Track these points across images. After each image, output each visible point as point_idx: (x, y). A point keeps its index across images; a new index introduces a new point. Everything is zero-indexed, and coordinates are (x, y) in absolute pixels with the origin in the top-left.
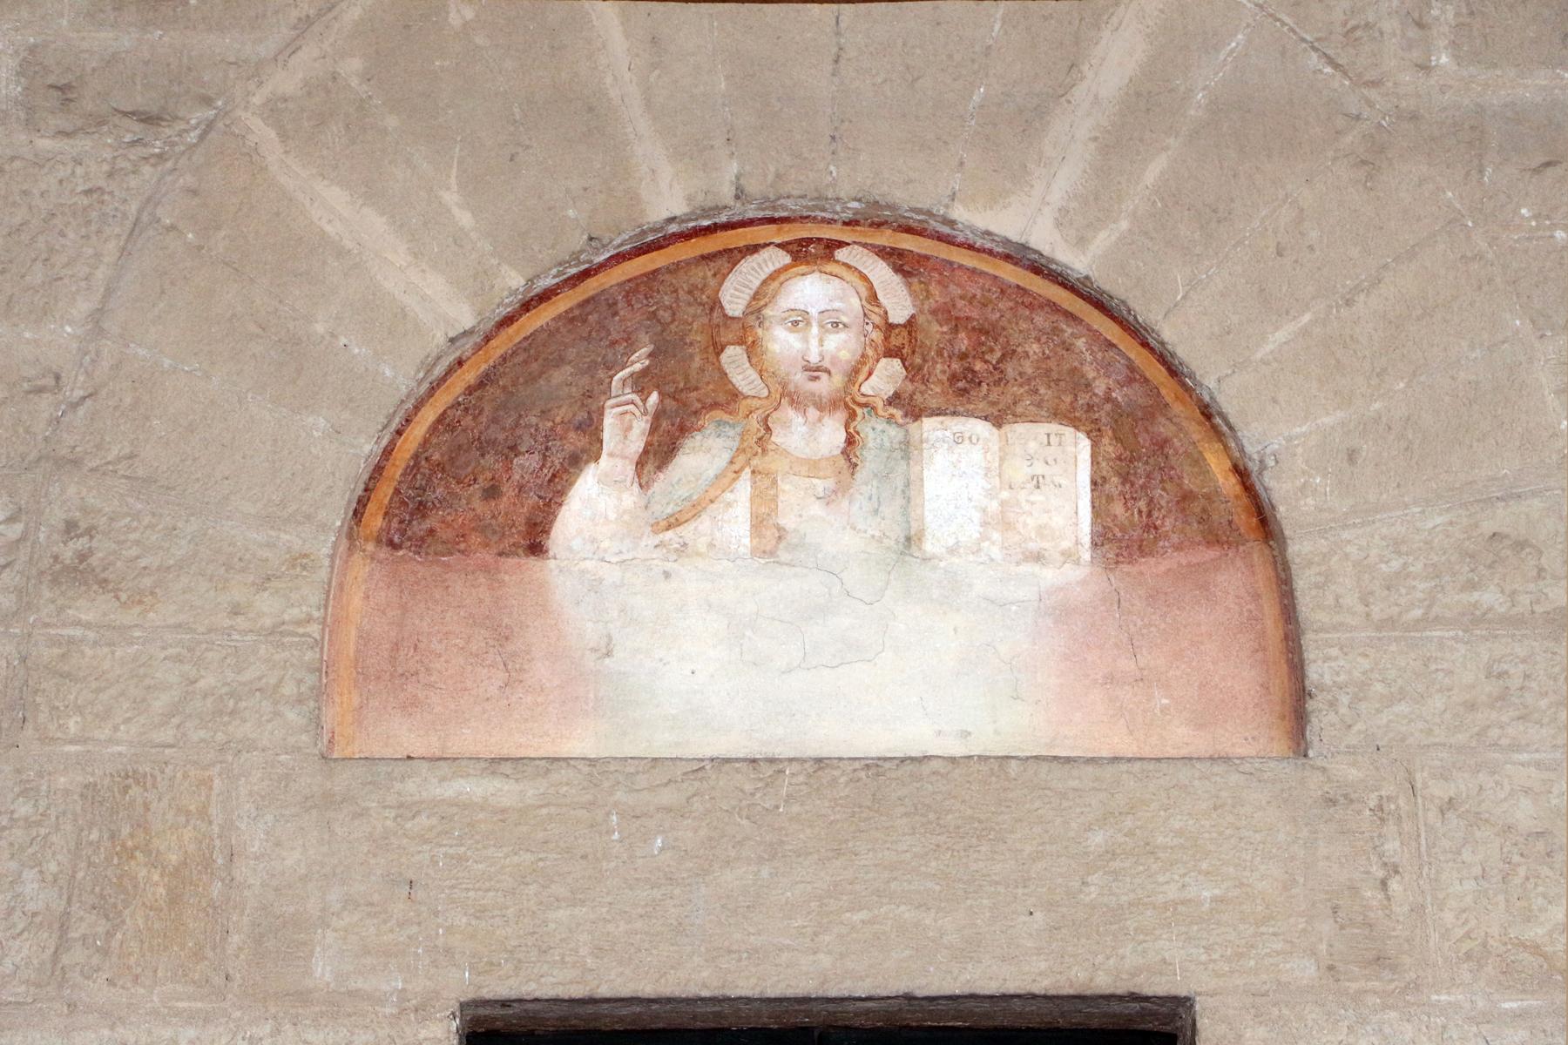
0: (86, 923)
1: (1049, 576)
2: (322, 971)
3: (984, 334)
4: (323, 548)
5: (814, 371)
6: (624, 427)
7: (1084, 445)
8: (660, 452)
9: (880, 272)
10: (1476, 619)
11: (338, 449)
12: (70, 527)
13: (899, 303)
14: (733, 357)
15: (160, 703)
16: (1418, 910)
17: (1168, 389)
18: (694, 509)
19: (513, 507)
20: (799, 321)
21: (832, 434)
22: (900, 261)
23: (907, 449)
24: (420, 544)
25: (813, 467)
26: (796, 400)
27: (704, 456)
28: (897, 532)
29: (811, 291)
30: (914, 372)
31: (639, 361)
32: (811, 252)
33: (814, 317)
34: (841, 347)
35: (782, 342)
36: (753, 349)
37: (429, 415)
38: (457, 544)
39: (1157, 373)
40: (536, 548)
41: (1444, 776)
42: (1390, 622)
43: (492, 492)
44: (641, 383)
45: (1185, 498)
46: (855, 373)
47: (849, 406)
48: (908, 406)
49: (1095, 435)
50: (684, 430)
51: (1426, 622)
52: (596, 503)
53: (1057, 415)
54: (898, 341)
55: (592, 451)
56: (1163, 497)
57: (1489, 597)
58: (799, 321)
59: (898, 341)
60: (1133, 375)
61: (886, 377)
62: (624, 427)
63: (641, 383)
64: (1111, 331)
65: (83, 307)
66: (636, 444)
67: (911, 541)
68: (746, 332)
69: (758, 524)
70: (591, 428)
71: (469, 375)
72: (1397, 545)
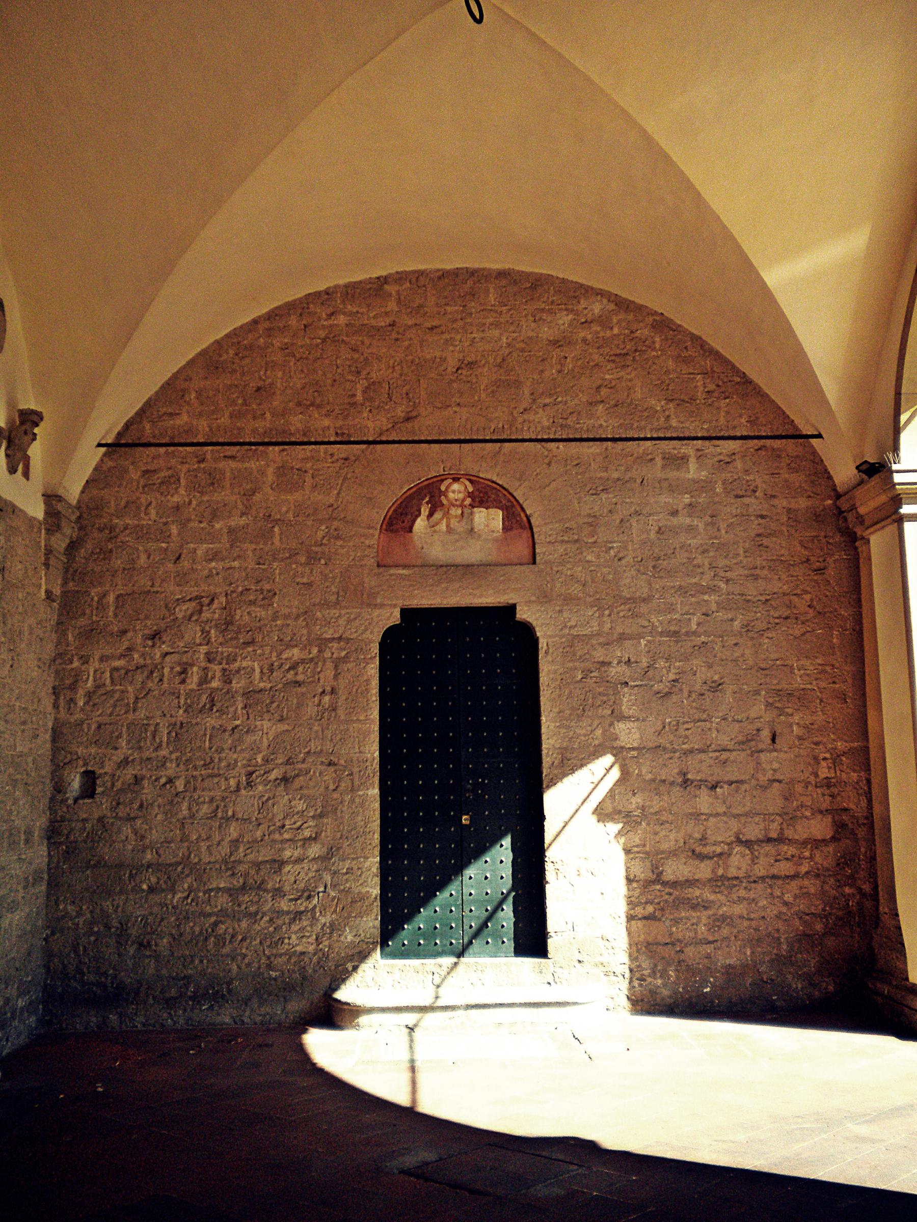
0: (341, 593)
1: (495, 535)
2: (379, 601)
3: (484, 494)
4: (377, 533)
5: (456, 500)
6: (425, 510)
7: (501, 513)
8: (430, 515)
9: (467, 483)
10: (563, 541)
11: (378, 516)
12: (336, 530)
13: (471, 489)
14: (443, 497)
15: (351, 558)
16: (551, 589)
17: (515, 503)
18: (437, 524)
19: (406, 524)
20: (454, 492)
21: (459, 512)
22: (471, 481)
23: (472, 513)
24: (392, 531)
25: (456, 517)
26: (454, 506)
27: (438, 515)
28: (469, 527)
29: (456, 486)
30: (473, 500)
31: (427, 499)
32: (456, 480)
33: (456, 491)
34: (461, 496)
35: (451, 495)
36: (446, 497)
37: (392, 509)
38: (397, 531)
39: (513, 500)
40: (411, 531)
41: (557, 566)
42: (549, 542)
43: (403, 522)
44: (427, 503)
45: (517, 520)
46: (464, 500)
47: (462, 506)
48: (472, 506)
49: (502, 510)
50: (435, 511)
51: (556, 542)
52: (420, 524)
53: (497, 507)
54: (470, 495)
55: (420, 515)
56: (514, 521)
57: (566, 538)
58: (454, 492)
59: (470, 495)
60: (509, 501)
61: (468, 501)
62: (425, 510)
63: (427, 503)
64: (506, 493)
65: (336, 492)
66: (427, 513)
67: (472, 529)
68: (445, 493)
69: (447, 526)
70: (419, 511)
71: (399, 502)
72: (551, 529)
